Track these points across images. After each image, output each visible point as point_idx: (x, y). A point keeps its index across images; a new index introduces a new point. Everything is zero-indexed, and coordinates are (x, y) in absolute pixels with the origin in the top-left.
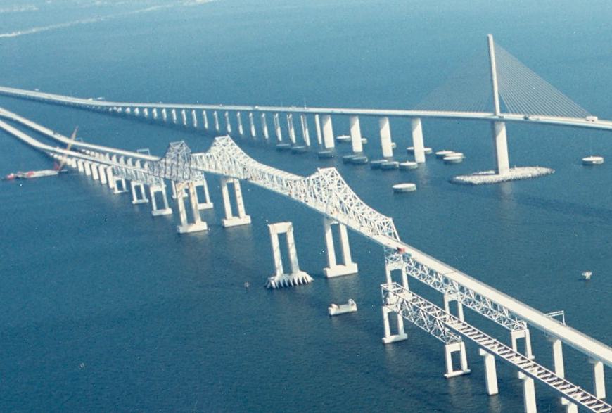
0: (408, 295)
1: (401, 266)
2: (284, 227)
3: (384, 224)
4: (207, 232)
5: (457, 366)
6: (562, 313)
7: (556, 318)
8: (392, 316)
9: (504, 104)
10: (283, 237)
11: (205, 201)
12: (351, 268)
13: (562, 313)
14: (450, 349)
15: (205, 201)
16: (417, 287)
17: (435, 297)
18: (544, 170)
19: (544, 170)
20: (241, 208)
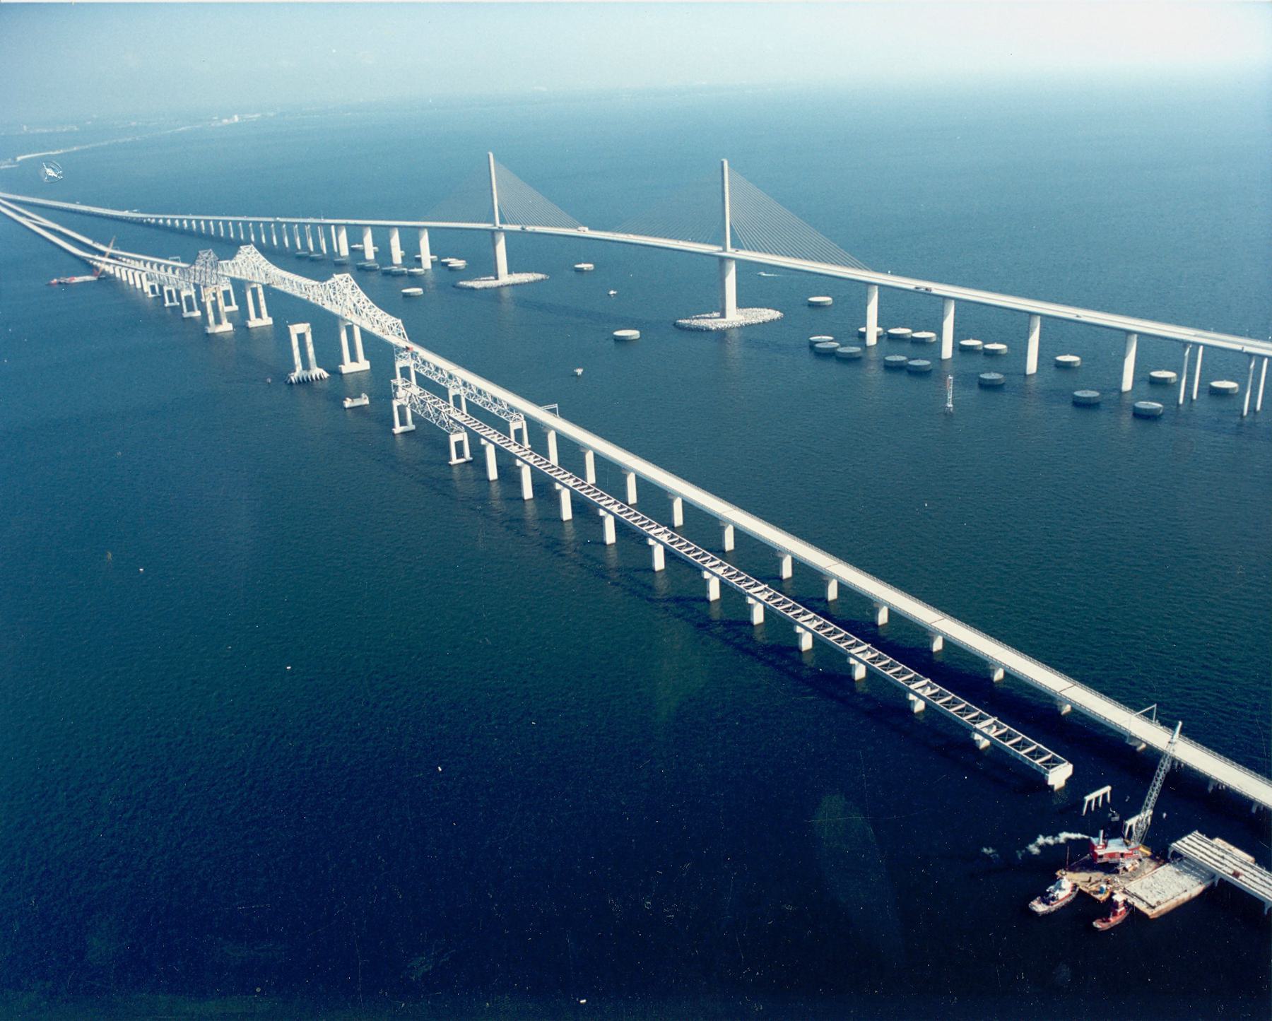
0: (415, 390)
1: (410, 363)
5: (460, 454)
6: (556, 406)
8: (402, 409)
12: (364, 365)
13: (556, 406)
14: (454, 438)
16: (423, 382)
20: (264, 310)
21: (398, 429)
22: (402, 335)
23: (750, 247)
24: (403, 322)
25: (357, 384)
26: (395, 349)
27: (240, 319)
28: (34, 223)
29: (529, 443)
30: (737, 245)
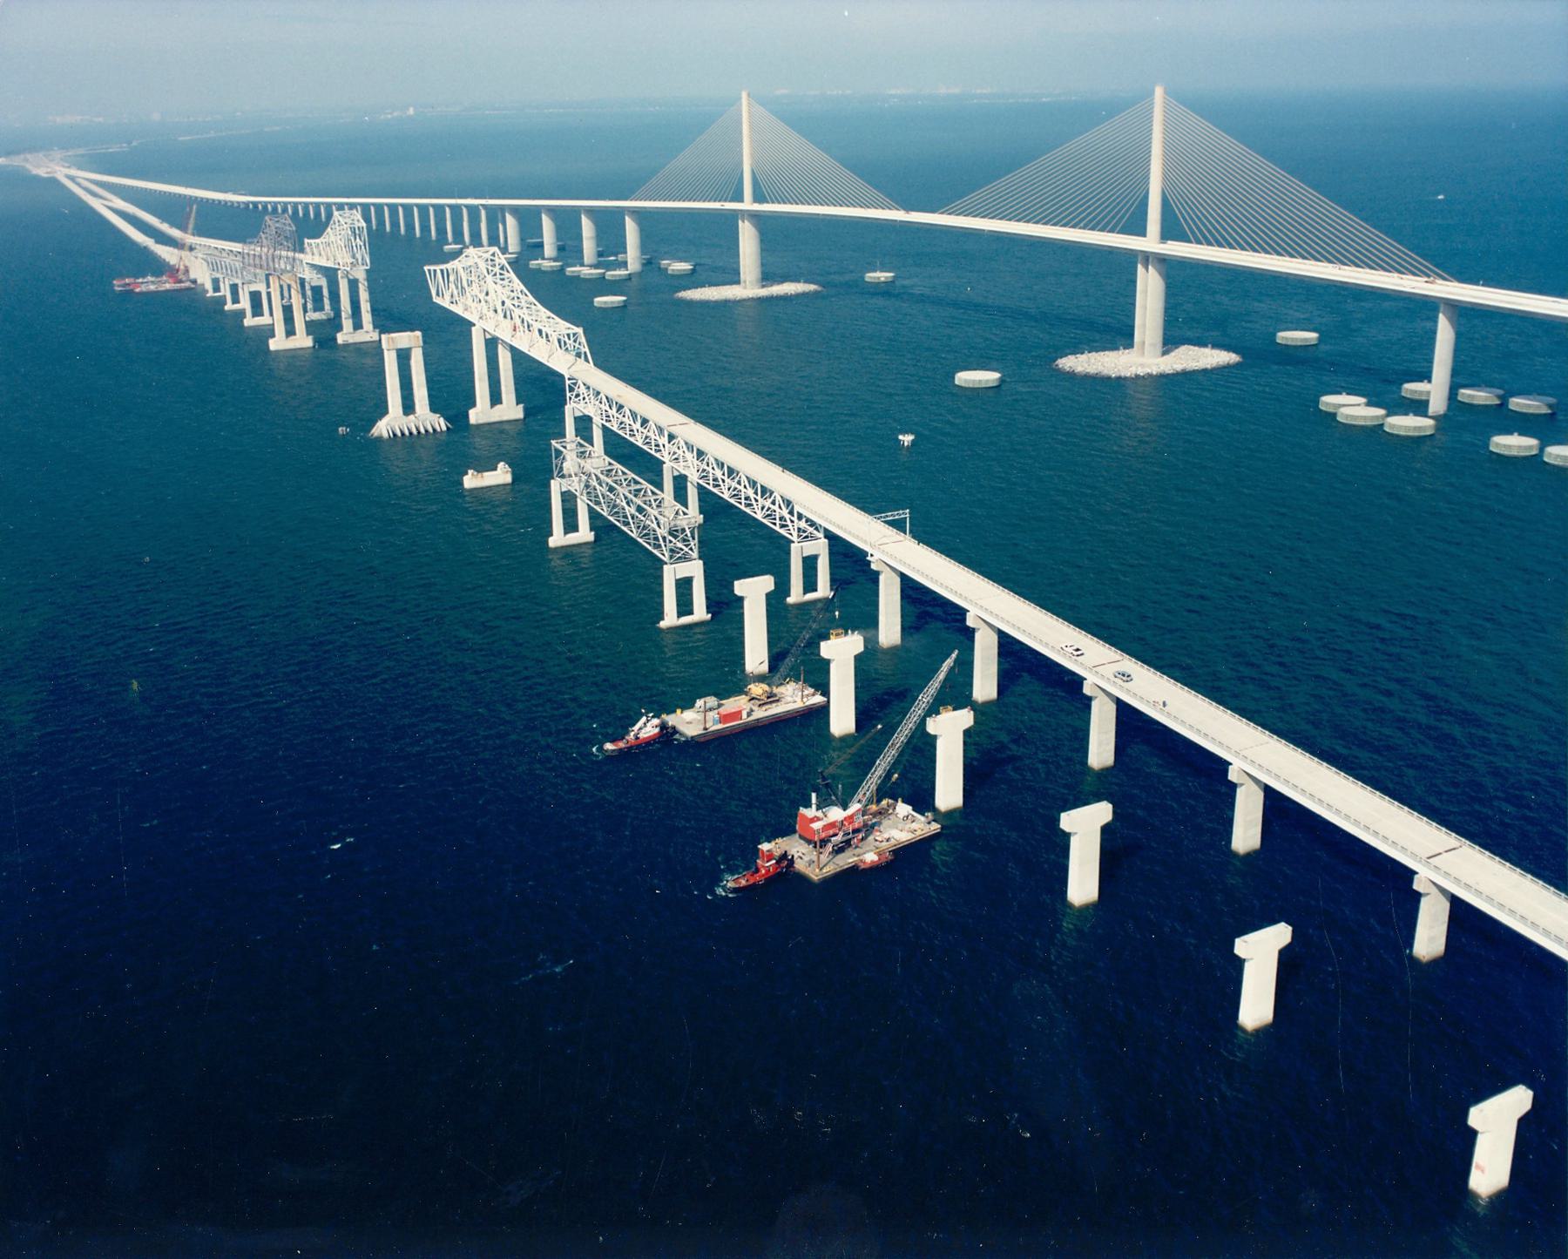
0: (598, 459)
1: (590, 409)
2: (410, 339)
3: (568, 335)
4: (311, 351)
5: (685, 607)
6: (906, 514)
7: (892, 524)
8: (569, 499)
9: (760, 187)
10: (404, 356)
11: (322, 309)
12: (509, 410)
13: (906, 514)
14: (671, 575)
15: (322, 309)
16: (618, 448)
17: (644, 464)
18: (812, 287)
19: (812, 287)
20: (367, 317)
21: (558, 539)
22: (583, 356)
23: (785, 200)
24: (585, 333)
25: (497, 437)
26: (568, 382)
27: (324, 333)
28: (107, 207)
29: (1060, 844)
30: (759, 197)
